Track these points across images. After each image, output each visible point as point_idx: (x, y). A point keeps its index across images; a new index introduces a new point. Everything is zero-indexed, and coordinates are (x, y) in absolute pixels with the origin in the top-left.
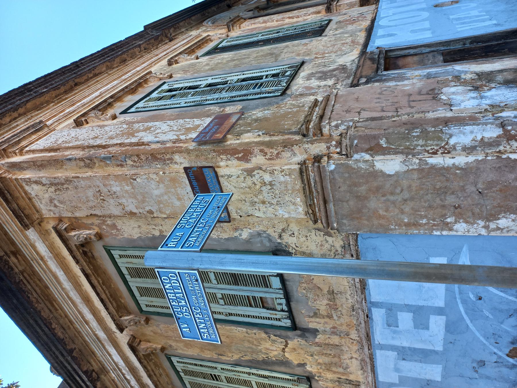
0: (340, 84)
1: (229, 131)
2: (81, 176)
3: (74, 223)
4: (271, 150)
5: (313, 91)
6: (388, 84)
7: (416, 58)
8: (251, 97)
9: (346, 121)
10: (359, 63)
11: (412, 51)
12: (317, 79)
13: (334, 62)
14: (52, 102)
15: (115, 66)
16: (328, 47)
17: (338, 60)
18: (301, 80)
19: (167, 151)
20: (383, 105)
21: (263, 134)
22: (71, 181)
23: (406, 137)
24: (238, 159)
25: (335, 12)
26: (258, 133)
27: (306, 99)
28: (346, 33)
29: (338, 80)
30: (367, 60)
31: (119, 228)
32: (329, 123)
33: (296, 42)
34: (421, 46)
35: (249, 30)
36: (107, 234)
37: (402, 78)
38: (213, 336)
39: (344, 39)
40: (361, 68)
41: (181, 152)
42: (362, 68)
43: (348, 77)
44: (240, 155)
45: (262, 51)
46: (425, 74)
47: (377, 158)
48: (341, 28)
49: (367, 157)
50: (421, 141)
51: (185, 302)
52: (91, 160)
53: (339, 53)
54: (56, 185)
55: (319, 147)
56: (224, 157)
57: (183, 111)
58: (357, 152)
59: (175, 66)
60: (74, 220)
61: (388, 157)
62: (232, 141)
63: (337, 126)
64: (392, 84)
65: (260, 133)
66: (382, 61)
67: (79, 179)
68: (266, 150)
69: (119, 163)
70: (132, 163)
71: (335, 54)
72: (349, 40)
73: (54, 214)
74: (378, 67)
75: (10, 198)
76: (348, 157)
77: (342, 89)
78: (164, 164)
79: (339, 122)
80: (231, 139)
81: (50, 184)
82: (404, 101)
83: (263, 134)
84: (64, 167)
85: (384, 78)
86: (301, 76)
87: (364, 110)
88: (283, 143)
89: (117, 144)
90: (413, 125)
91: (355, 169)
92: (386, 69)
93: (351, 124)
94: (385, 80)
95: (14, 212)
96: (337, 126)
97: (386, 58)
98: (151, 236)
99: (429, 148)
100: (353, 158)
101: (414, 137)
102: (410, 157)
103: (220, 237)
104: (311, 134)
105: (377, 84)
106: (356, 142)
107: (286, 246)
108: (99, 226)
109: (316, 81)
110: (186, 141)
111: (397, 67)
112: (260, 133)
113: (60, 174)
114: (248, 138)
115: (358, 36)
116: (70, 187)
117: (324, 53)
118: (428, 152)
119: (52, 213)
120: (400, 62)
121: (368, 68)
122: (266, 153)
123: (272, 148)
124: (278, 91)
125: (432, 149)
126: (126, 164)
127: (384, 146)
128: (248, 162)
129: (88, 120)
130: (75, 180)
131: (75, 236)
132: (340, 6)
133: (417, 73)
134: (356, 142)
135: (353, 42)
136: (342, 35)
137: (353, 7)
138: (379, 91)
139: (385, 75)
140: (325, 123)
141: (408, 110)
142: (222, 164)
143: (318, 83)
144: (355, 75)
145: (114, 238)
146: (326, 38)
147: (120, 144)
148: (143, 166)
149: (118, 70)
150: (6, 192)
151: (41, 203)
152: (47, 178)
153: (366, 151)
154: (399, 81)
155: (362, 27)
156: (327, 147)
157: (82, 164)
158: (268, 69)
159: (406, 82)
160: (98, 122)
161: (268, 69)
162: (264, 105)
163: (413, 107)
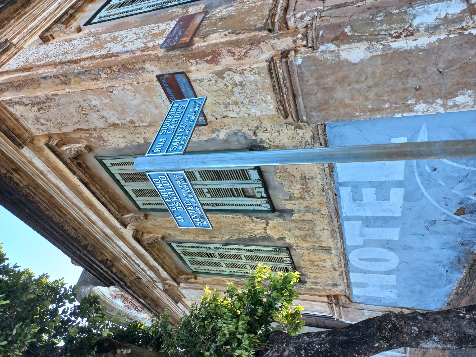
1: (195, 33)
2: (59, 93)
3: (64, 139)
4: (238, 50)
9: (311, 11)
21: (229, 33)
22: (51, 99)
23: (370, 23)
24: (208, 62)
26: (224, 33)
31: (105, 139)
32: (294, 15)
38: (205, 224)
44: (209, 58)
47: (342, 47)
50: (385, 25)
56: (193, 61)
58: (323, 43)
60: (62, 136)
61: (353, 45)
62: (199, 44)
63: (302, 18)
65: (226, 32)
68: (234, 50)
69: (94, 77)
70: (106, 76)
76: (314, 49)
78: (137, 74)
79: (304, 13)
80: (198, 42)
89: (87, 58)
96: (302, 18)
98: (137, 144)
99: (393, 32)
100: (319, 50)
101: (378, 21)
102: (374, 43)
103: (200, 139)
104: (277, 28)
107: (260, 142)
110: (154, 48)
114: (215, 38)
123: (240, 47)
125: (395, 33)
126: (101, 78)
127: (349, 34)
131: (67, 150)
134: (321, 32)
148: (116, 78)
153: (332, 41)
156: (293, 41)
157: (58, 81)
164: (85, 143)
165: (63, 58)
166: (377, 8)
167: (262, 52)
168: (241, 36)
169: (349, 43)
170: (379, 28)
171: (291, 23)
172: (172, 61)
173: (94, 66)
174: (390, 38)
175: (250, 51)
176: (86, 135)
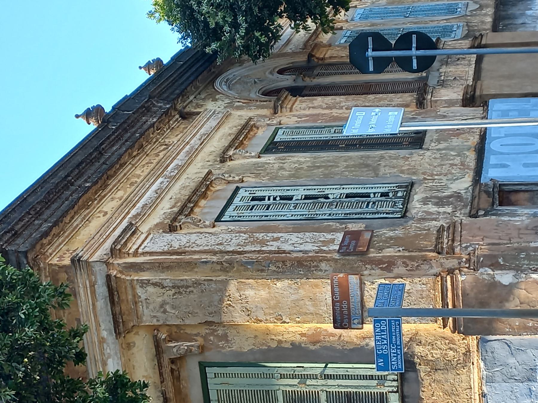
0: (459, 213)
1: (369, 246)
2: (214, 279)
3: (174, 334)
4: (412, 263)
5: (434, 216)
6: (503, 218)
7: (527, 195)
8: (368, 216)
9: (474, 244)
10: (473, 192)
11: (523, 188)
12: (434, 205)
13: (446, 187)
14: (95, 199)
15: (135, 153)
16: (435, 167)
17: (451, 186)
18: (417, 204)
19: (313, 259)
20: (500, 235)
21: (403, 250)
22: (200, 284)
23: (516, 258)
24: (382, 269)
25: (429, 108)
26: (398, 249)
27: (430, 224)
28: (452, 150)
29: (456, 208)
30: (483, 192)
31: (229, 339)
32: (460, 245)
33: (392, 152)
34: (532, 184)
35: (307, 116)
36: (212, 346)
37: (515, 215)
38: (400, 367)
39: (452, 158)
40: (477, 198)
41: (328, 260)
42: (479, 198)
43: (465, 206)
44: (384, 266)
45: (350, 158)
46: (532, 212)
47: (496, 272)
48: (445, 140)
49: (490, 272)
50: (526, 261)
51: (387, 342)
52: (230, 264)
53: (450, 176)
54: (179, 287)
55: (452, 262)
56: (368, 266)
57: (299, 224)
58: (482, 267)
59: (229, 163)
60: (175, 329)
61: (505, 271)
62: (373, 254)
63: (466, 247)
64: (506, 218)
65: (401, 249)
66: (497, 195)
67: (210, 282)
68: (408, 262)
69: (261, 268)
70: (275, 269)
71: (446, 178)
72: (457, 160)
73: (158, 321)
74: (493, 200)
75: (116, 299)
76: (475, 270)
77: (461, 216)
78: (308, 271)
79: (469, 244)
80: (373, 252)
81: (173, 286)
82: (515, 233)
83: (403, 250)
84: (196, 270)
85: (499, 212)
86: (415, 200)
87: (486, 237)
88: (422, 257)
89: (255, 251)
90: (521, 250)
91: (480, 279)
92: (500, 205)
93: (477, 246)
94: (500, 215)
95: (114, 315)
96: (466, 247)
97: (501, 191)
98: (266, 348)
99: (532, 267)
100: (479, 272)
101: (522, 258)
102: (519, 272)
103: (345, 348)
104: (445, 252)
105: (494, 217)
106: (482, 259)
107: (411, 356)
108: (205, 338)
109: (434, 207)
110: (330, 252)
111: (510, 203)
112: (401, 249)
113: (188, 277)
114: (389, 252)
115: (467, 157)
116: (195, 291)
117: (432, 175)
118: (531, 269)
119: (155, 320)
120: (513, 197)
121: (485, 201)
122: (408, 265)
123: (413, 261)
124: (397, 212)
125: (533, 267)
126: (268, 269)
127: (502, 263)
128: (390, 272)
129: (182, 226)
130: (206, 283)
131: (174, 347)
132: (436, 101)
133: (526, 211)
134: (482, 259)
135: (462, 164)
136: (448, 151)
137: (453, 106)
138: (496, 223)
139: (500, 210)
140: (456, 244)
141: (519, 240)
142: (366, 273)
143: (437, 209)
144: (471, 205)
145: (219, 351)
146: (428, 153)
147: (259, 252)
148: (285, 272)
149: (139, 159)
150: (116, 293)
151: (147, 308)
152: (171, 280)
153: (489, 266)
154: (512, 217)
155: (469, 143)
156: (459, 263)
157: (219, 267)
158: (373, 186)
159: (517, 219)
160: (194, 228)
161: (373, 186)
162: (388, 226)
163: (521, 238)
164: (200, 341)
165: (216, 248)
166: (520, 249)
167: (432, 267)
168: (413, 254)
169: (501, 270)
170: (523, 262)
171: (457, 250)
172: (348, 264)
173: (263, 258)
174: (530, 271)
175: (422, 266)
176: (207, 331)
